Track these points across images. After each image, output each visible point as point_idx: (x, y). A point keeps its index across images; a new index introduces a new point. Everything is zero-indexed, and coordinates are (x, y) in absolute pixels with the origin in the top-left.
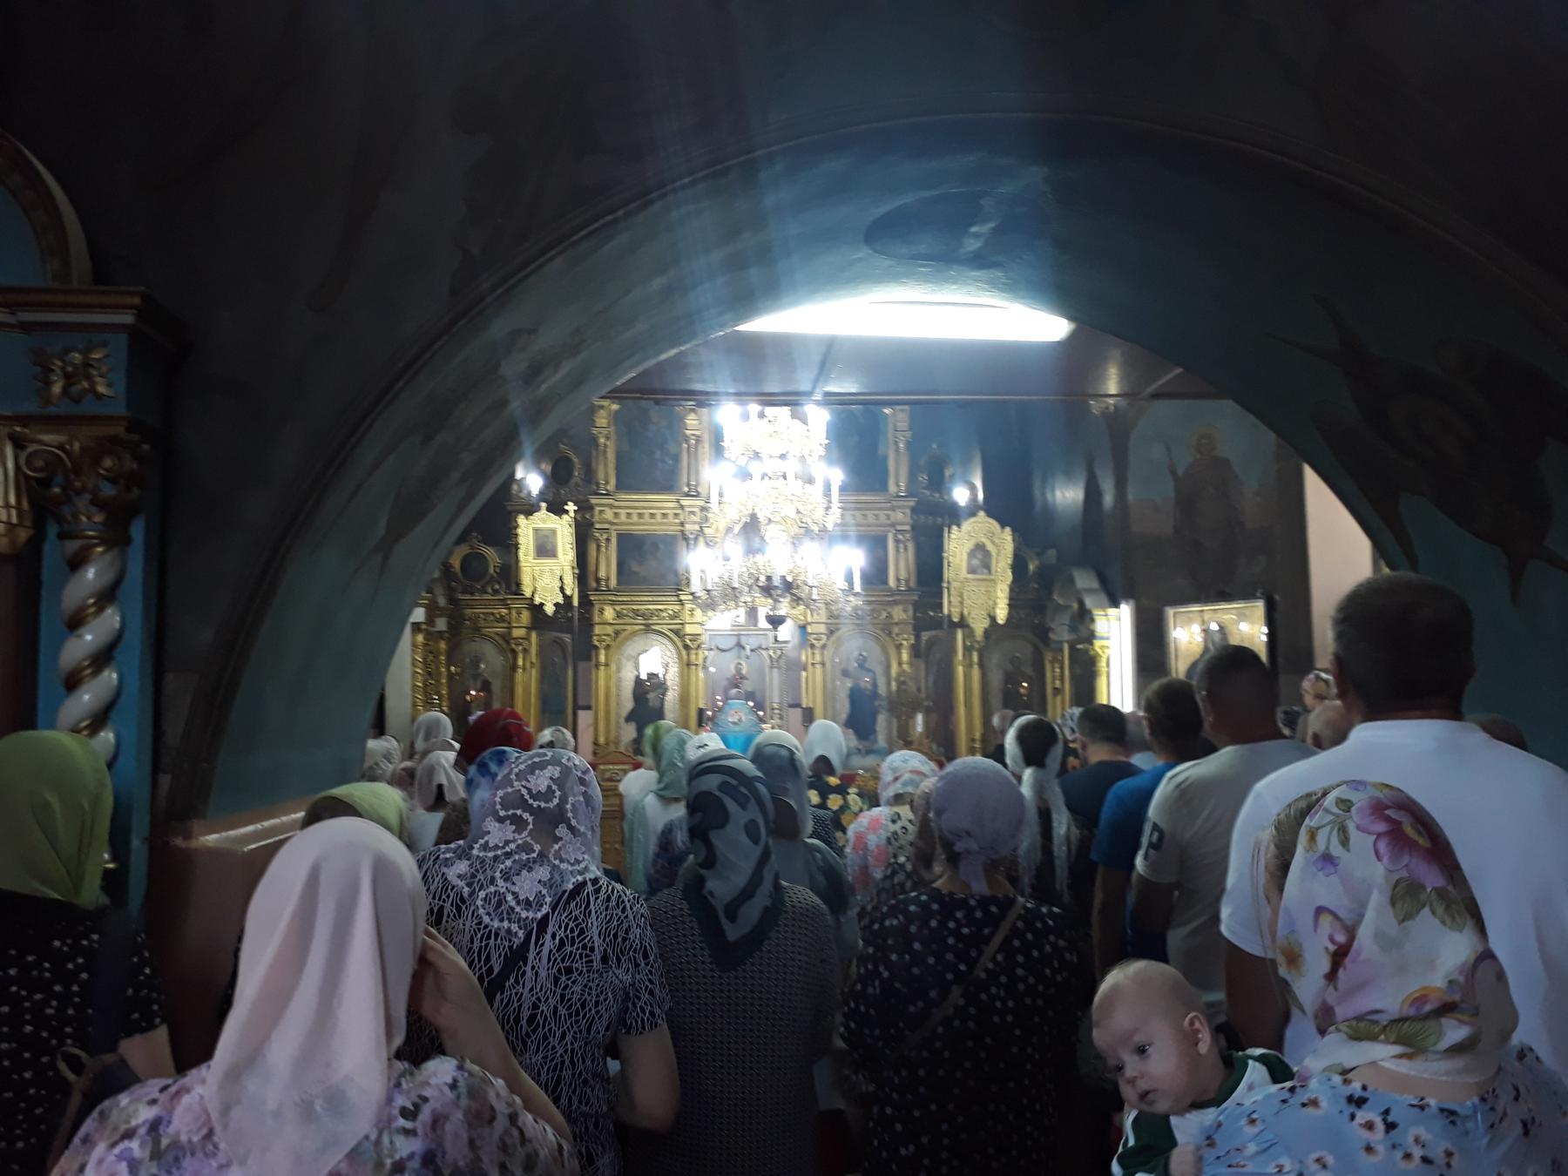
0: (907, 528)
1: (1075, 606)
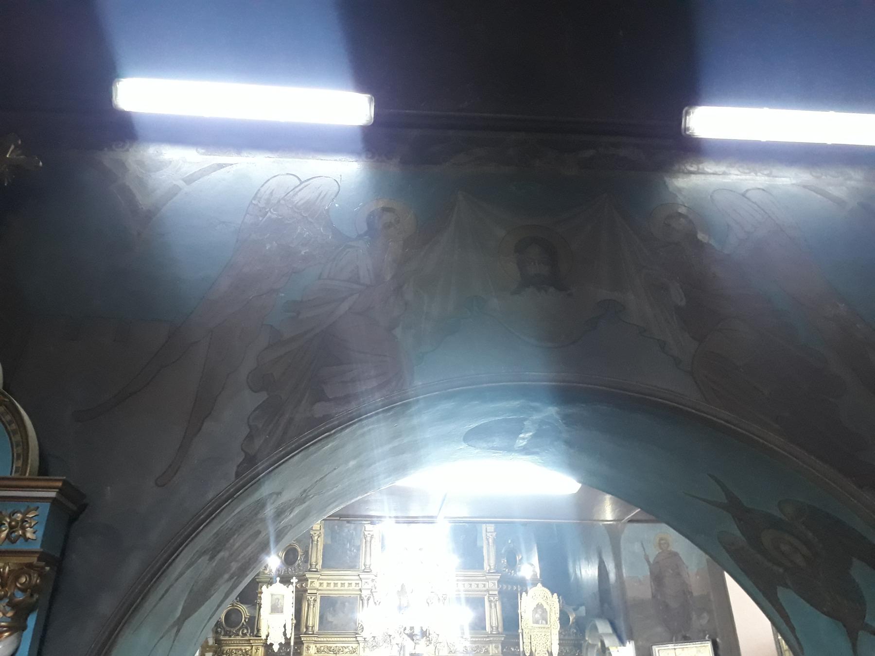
0: (496, 593)
1: (599, 644)
